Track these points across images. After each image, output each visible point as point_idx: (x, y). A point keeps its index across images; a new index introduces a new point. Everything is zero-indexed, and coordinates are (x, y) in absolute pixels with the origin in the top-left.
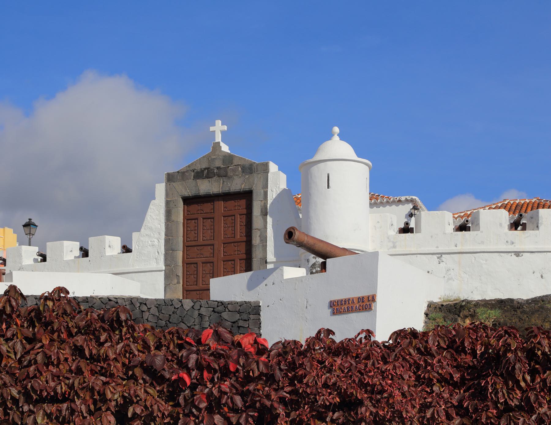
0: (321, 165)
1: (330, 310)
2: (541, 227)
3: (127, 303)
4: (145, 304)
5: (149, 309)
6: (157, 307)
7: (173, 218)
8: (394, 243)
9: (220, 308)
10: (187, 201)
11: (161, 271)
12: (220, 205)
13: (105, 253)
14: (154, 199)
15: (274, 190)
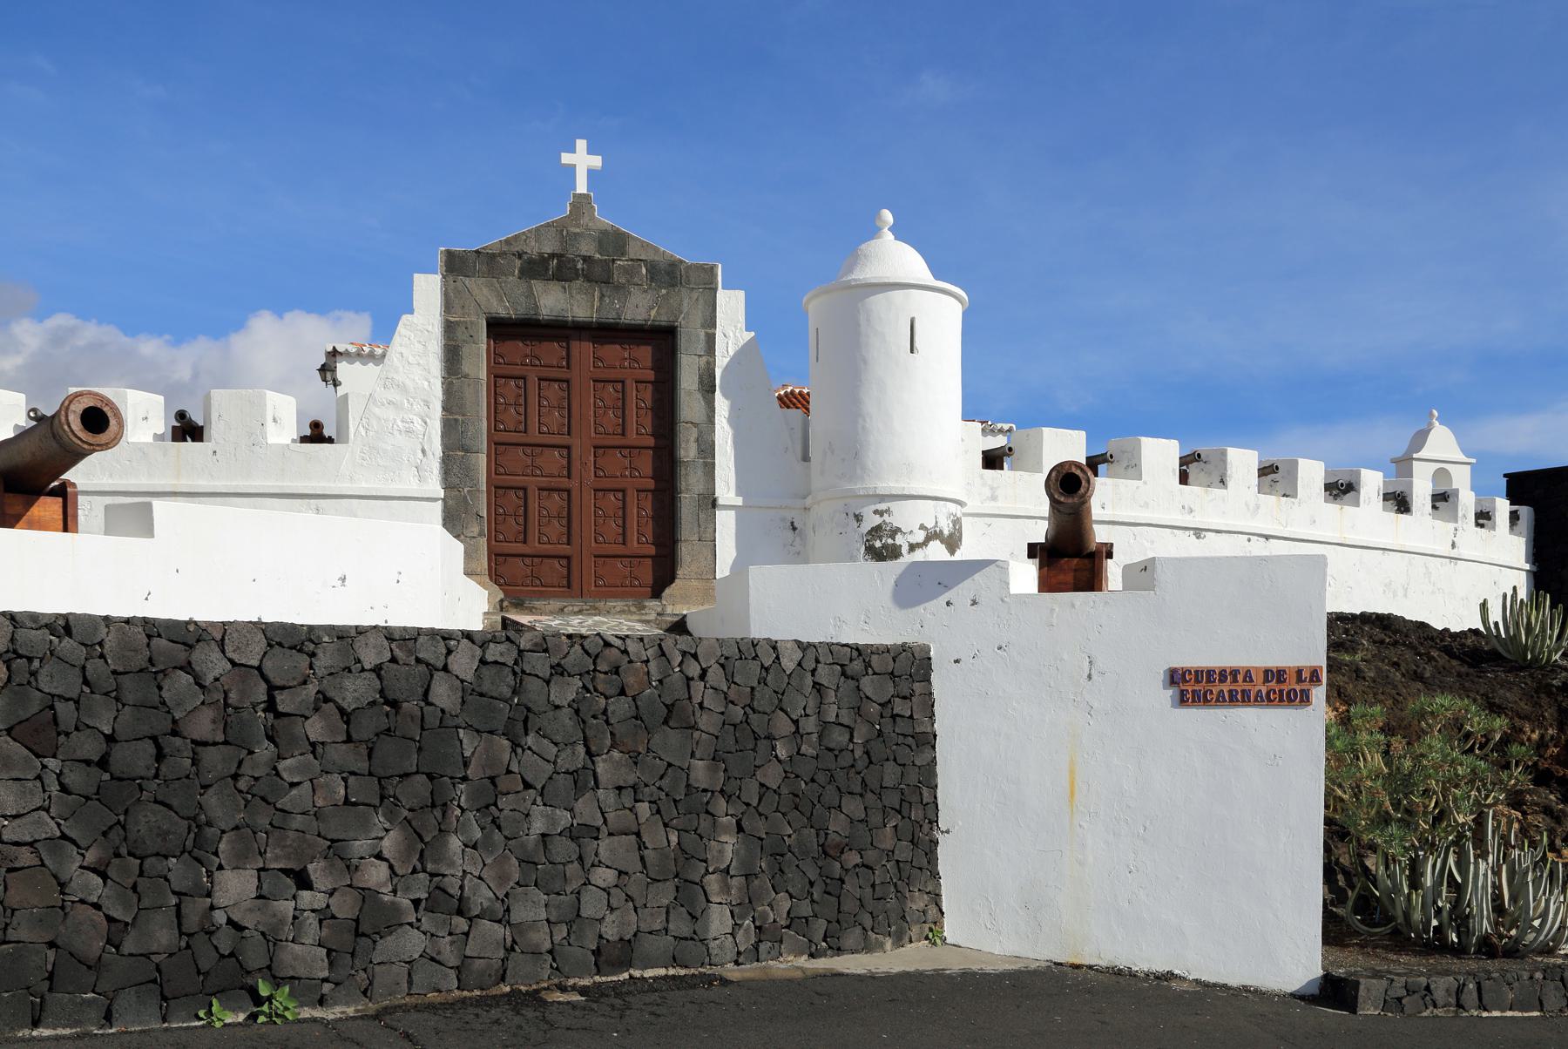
0: (897, 295)
1: (1170, 692)
2: (1230, 483)
3: (650, 652)
4: (695, 656)
5: (704, 673)
6: (722, 666)
7: (466, 367)
9: (857, 666)
10: (499, 329)
11: (435, 500)
12: (584, 350)
13: (264, 437)
14: (411, 312)
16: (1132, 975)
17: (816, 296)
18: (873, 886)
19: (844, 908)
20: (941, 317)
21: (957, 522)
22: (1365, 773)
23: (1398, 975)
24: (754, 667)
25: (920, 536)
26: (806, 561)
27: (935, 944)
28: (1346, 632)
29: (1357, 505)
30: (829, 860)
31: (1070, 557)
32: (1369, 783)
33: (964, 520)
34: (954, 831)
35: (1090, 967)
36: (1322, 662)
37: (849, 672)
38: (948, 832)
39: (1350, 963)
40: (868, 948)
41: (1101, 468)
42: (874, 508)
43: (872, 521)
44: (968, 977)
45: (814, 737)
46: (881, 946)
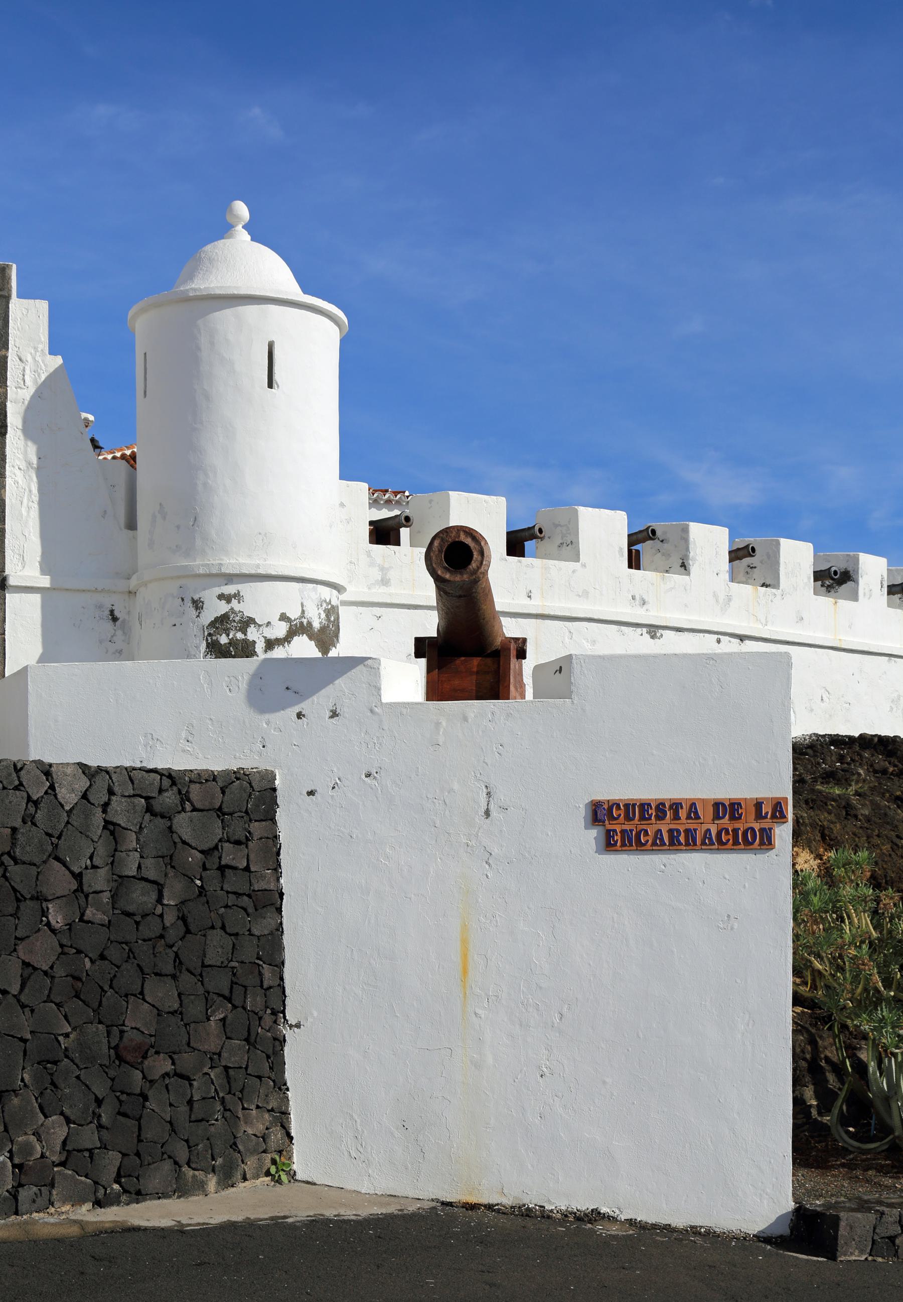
0: (250, 311)
2: (694, 569)
8: (382, 569)
15: (29, 358)
16: (545, 1215)
17: (143, 310)
18: (190, 1102)
19: (148, 1135)
20: (312, 344)
21: (332, 612)
22: (847, 937)
23: (891, 1206)
24: (18, 800)
25: (281, 630)
26: (131, 658)
27: (279, 1181)
28: (841, 759)
29: (855, 597)
30: (125, 1068)
31: (468, 655)
32: (853, 952)
33: (342, 611)
34: (307, 1025)
35: (490, 1207)
36: (784, 789)
37: (157, 808)
38: (298, 1026)
39: (833, 1189)
40: (182, 1190)
41: (529, 545)
42: (218, 591)
43: (215, 609)
44: (318, 1226)
45: (106, 898)
46: (201, 1187)
